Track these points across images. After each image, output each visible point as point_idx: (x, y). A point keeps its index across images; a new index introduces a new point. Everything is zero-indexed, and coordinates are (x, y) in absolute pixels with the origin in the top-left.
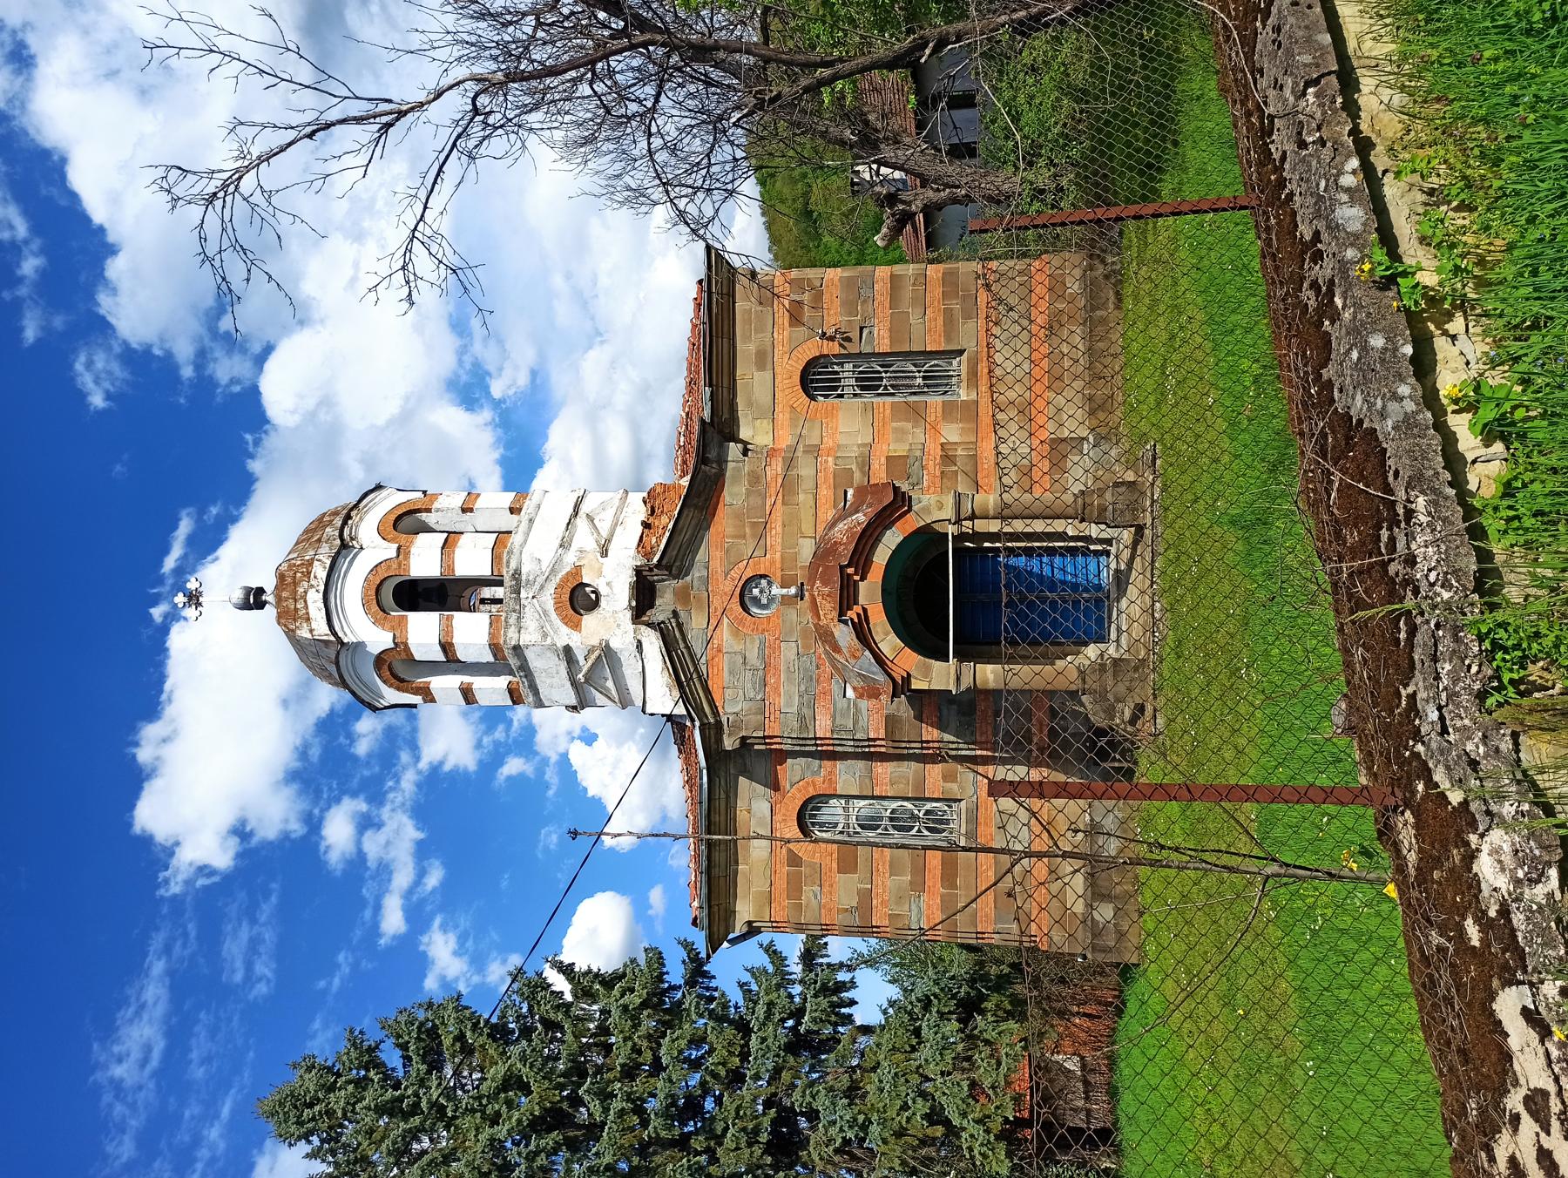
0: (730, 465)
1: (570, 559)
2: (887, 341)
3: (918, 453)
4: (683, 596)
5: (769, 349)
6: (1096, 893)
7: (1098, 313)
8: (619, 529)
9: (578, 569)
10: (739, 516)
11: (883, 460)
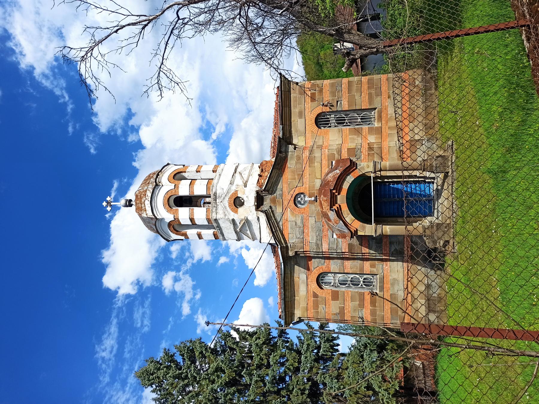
0: (290, 153)
1: (234, 188)
2: (347, 106)
4: (274, 201)
5: (303, 110)
8: (250, 177)
10: (293, 172)
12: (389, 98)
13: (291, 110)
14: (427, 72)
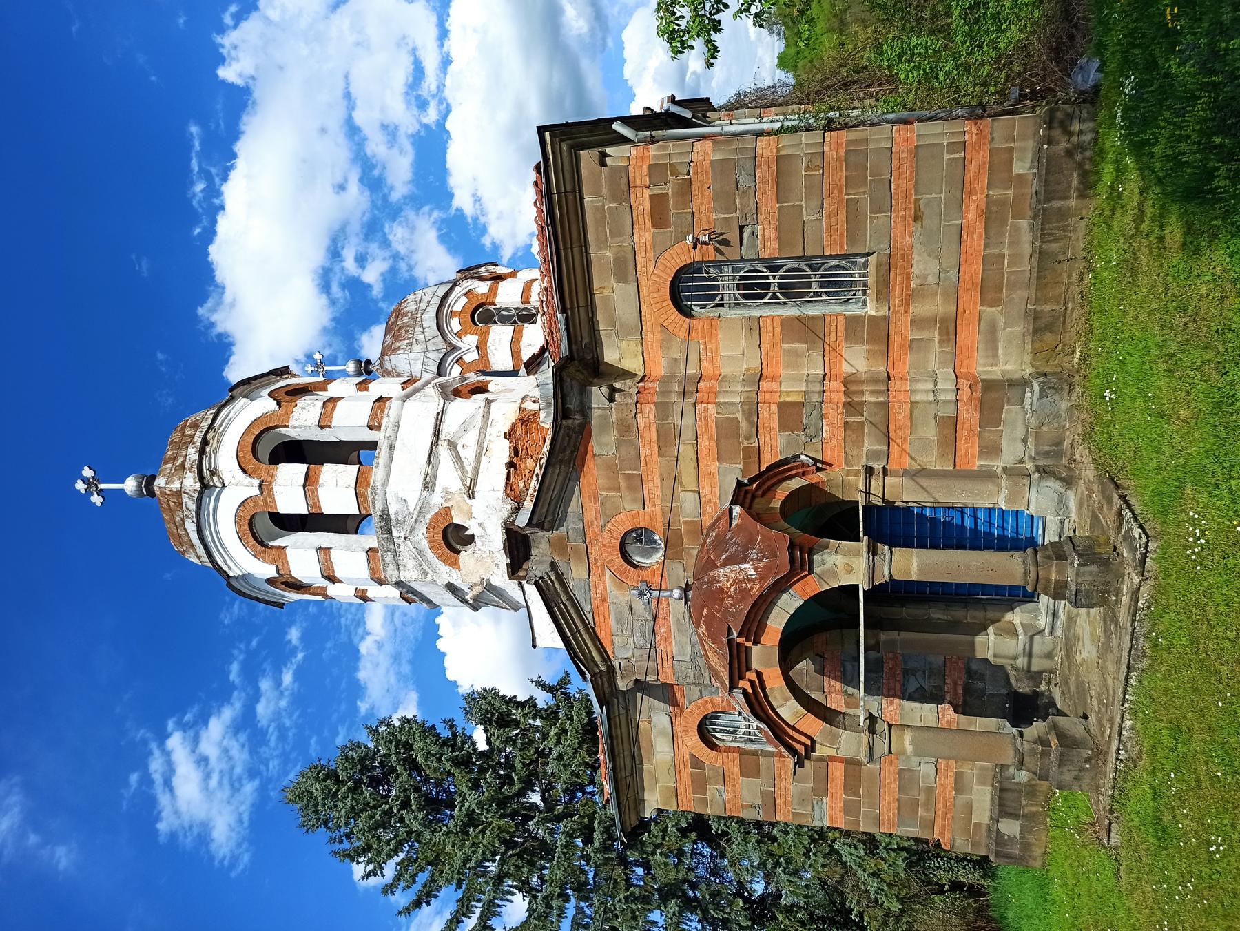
0: (596, 413)
1: (437, 499)
2: (774, 244)
3: (816, 398)
4: (560, 546)
5: (630, 256)
6: (1003, 809)
7: (1056, 204)
8: (484, 459)
9: (446, 511)
10: (610, 468)
11: (774, 408)
12: (916, 219)
13: (587, 253)
14: (1057, 133)
